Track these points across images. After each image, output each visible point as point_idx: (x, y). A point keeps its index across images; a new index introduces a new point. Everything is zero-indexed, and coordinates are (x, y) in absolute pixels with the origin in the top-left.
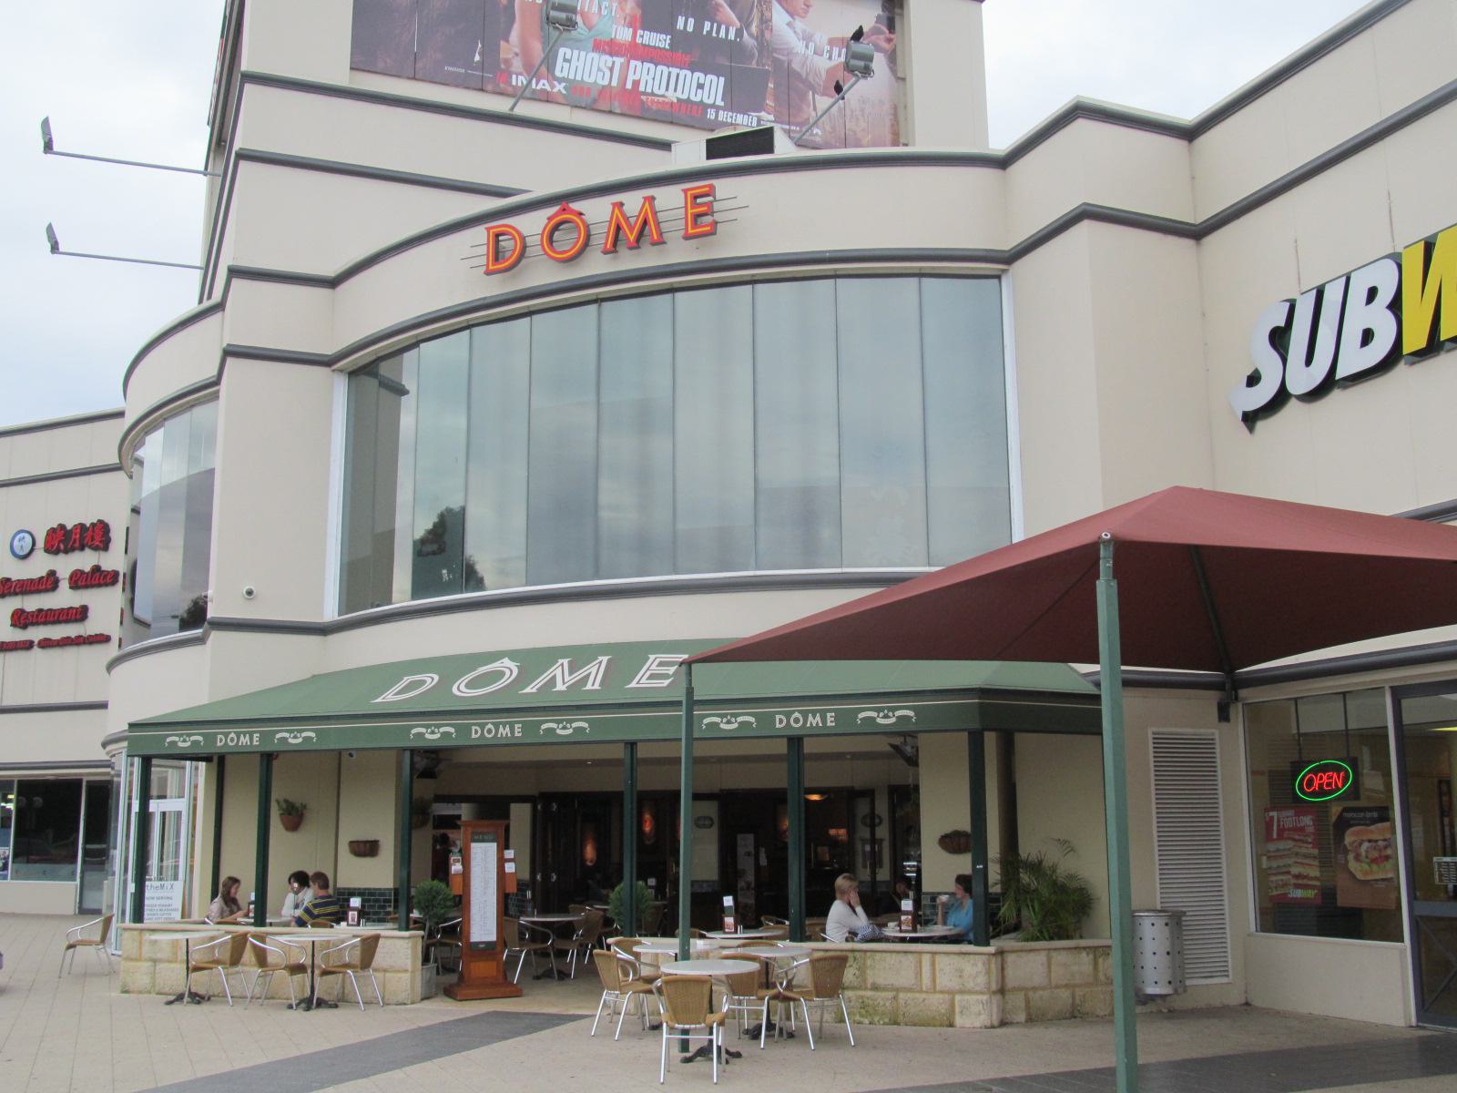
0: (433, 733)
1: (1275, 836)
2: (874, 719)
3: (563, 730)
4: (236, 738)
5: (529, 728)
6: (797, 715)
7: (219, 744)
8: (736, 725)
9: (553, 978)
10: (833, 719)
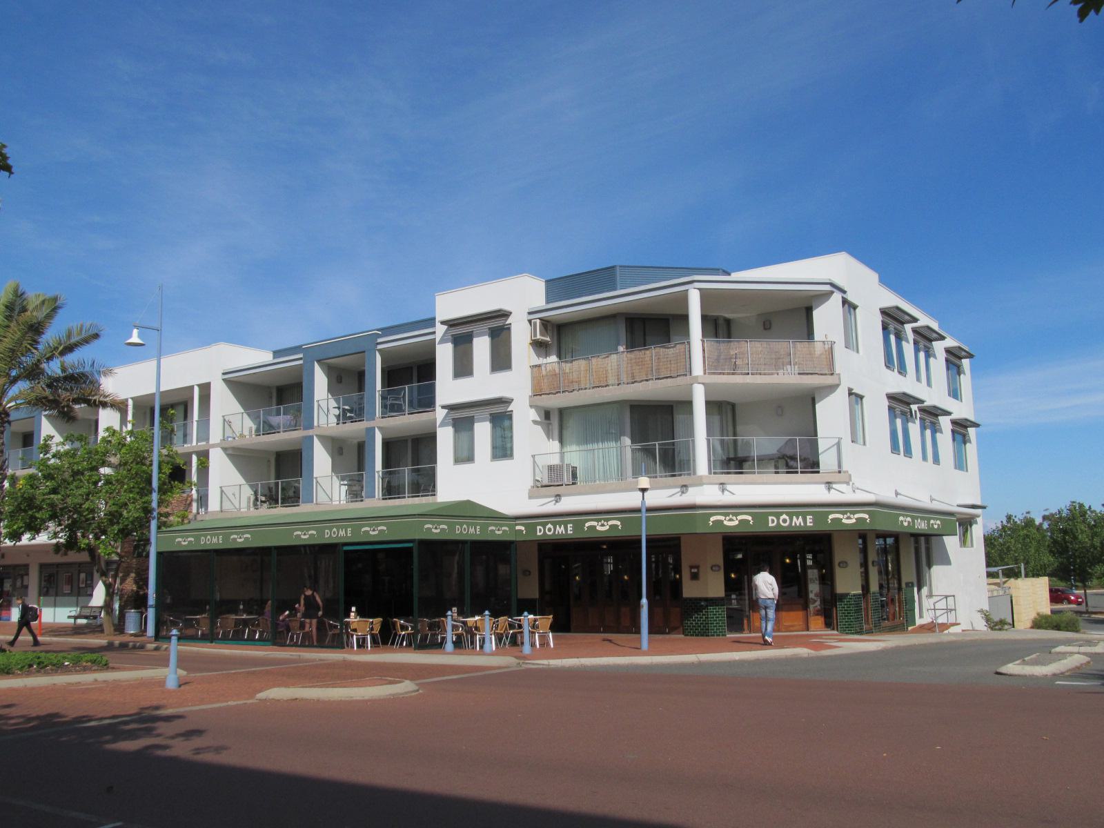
0: (603, 525)
1: (194, 458)
2: (595, 527)
3: (602, 528)
4: (788, 520)
5: (356, 530)
6: (784, 516)
7: (326, 536)
8: (737, 522)
9: (434, 467)
10: (811, 520)
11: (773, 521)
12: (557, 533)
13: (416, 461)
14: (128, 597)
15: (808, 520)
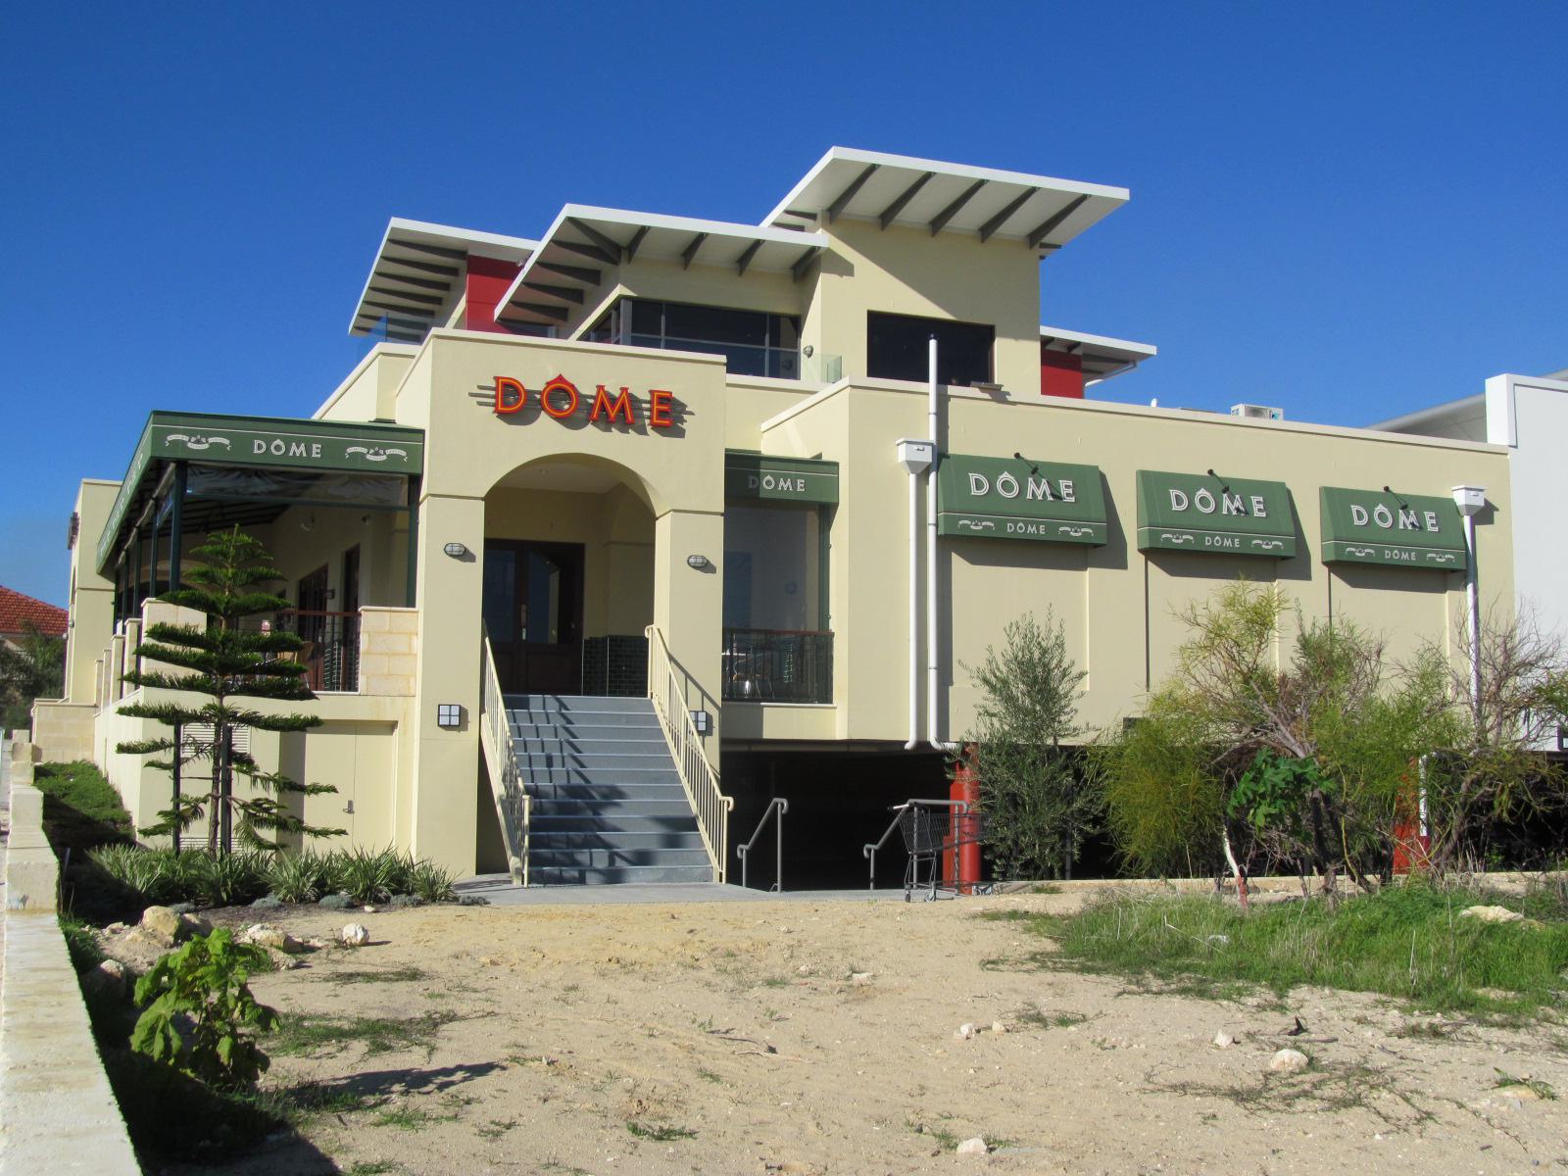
1: (172, 466)
6: (1021, 524)
11: (260, 447)
12: (291, 454)
13: (775, 342)
14: (1229, 755)
15: (314, 450)
